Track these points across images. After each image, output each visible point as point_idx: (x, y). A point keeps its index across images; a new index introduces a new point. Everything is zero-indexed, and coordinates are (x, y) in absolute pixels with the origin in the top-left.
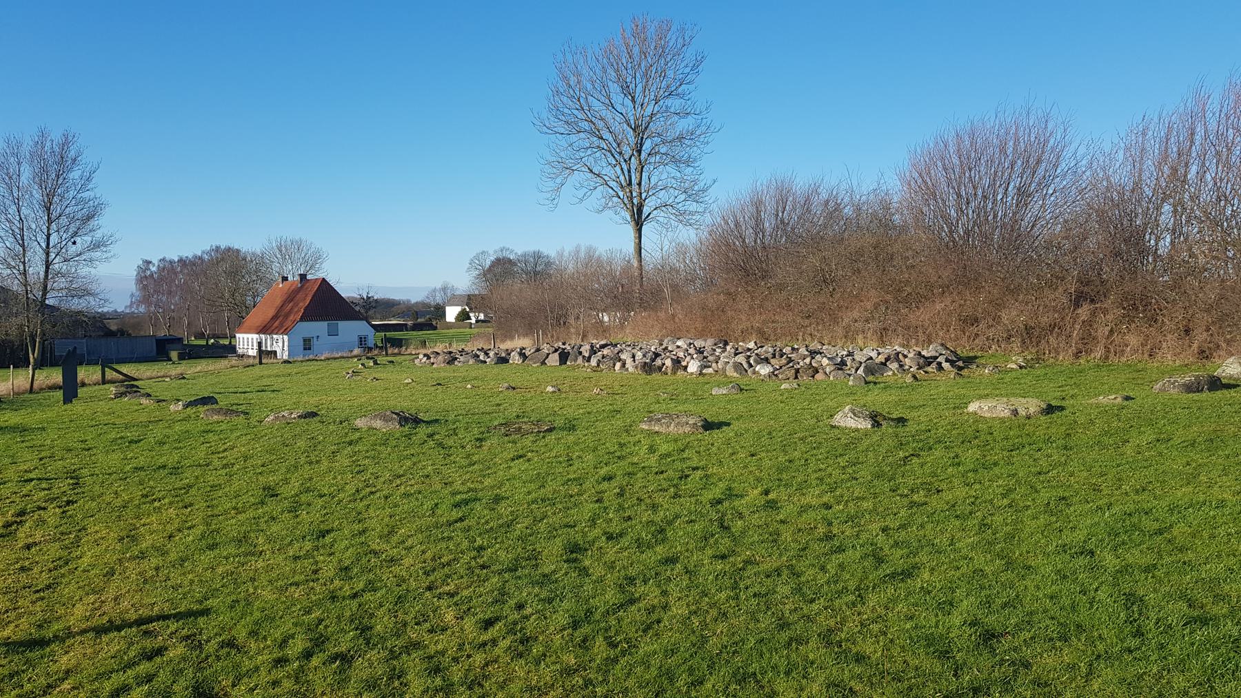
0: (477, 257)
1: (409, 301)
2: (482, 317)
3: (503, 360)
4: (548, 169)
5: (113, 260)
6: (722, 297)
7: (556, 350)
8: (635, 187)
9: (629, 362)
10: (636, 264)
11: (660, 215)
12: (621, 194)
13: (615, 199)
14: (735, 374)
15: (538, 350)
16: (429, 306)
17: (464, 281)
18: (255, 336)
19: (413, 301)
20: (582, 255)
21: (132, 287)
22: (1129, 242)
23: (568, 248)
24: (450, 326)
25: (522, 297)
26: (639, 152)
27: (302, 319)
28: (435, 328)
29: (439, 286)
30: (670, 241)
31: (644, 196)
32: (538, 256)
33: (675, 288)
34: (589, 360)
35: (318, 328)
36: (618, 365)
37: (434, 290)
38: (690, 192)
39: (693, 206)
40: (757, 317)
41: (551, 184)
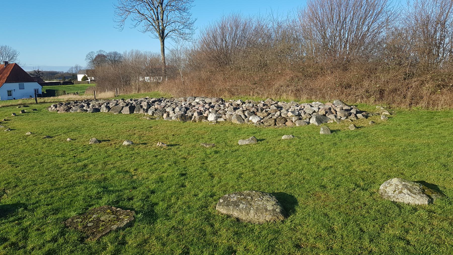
1: (62, 72)
2: (93, 78)
3: (97, 110)
4: (118, 11)
7: (127, 105)
8: (160, 20)
10: (162, 58)
11: (173, 34)
12: (154, 24)
13: (151, 27)
14: (238, 122)
15: (117, 105)
16: (70, 74)
17: (84, 64)
19: (64, 72)
20: (134, 54)
22: (431, 45)
23: (128, 51)
24: (79, 83)
25: (111, 72)
26: (162, 4)
27: (6, 82)
28: (73, 84)
29: (74, 66)
30: (181, 46)
31: (165, 25)
32: (115, 54)
34: (147, 111)
35: (14, 86)
36: (165, 115)
37: (72, 68)
38: (185, 24)
39: (187, 31)
40: (228, 83)
41: (120, 18)
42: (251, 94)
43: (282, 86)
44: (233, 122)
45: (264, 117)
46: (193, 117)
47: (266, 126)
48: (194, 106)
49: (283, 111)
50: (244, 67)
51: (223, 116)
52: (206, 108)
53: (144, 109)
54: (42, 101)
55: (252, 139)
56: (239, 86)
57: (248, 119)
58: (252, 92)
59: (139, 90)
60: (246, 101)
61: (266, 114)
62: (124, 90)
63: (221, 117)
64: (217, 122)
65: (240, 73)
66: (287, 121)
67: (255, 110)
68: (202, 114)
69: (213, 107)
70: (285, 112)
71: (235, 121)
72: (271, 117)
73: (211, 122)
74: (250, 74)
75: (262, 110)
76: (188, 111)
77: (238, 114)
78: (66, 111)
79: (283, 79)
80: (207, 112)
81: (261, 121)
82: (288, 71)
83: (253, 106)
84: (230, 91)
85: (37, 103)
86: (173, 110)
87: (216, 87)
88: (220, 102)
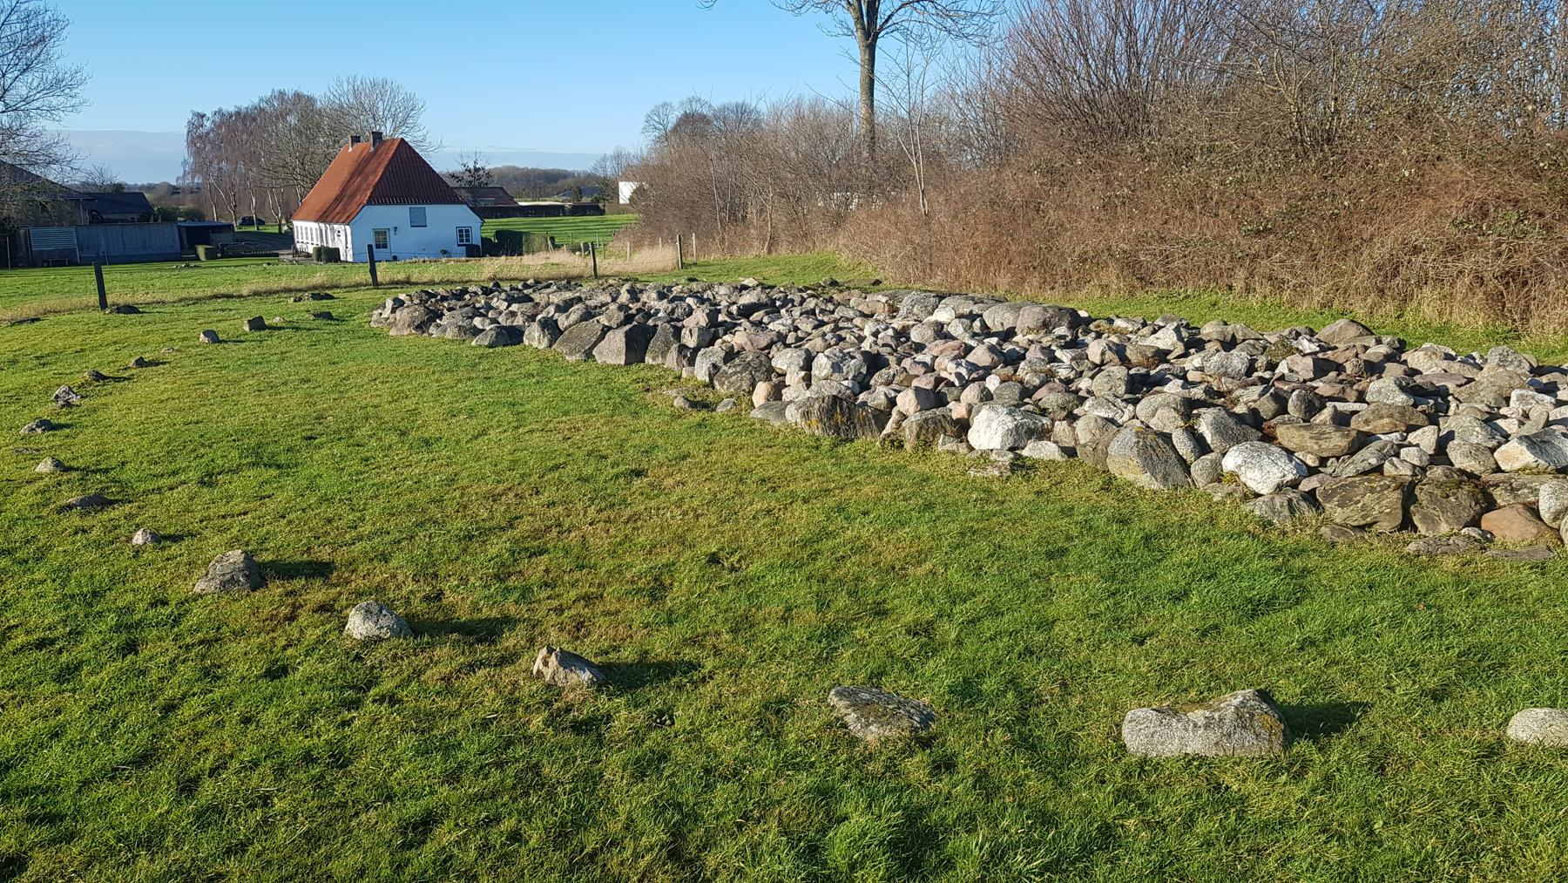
0: (656, 112)
5: (83, 108)
6: (1036, 178)
9: (794, 390)
14: (1145, 480)
17: (637, 142)
18: (315, 225)
21: (182, 152)
24: (622, 210)
27: (371, 201)
28: (602, 212)
29: (610, 152)
32: (742, 111)
33: (933, 158)
35: (395, 215)
36: (762, 390)
37: (604, 159)
40: (1122, 228)
42: (1239, 285)
43: (1416, 250)
44: (1113, 469)
45: (1323, 461)
46: (895, 416)
47: (1343, 528)
48: (920, 348)
49: (1462, 420)
50: (1211, 150)
51: (1061, 427)
52: (973, 367)
53: (683, 348)
54: (401, 276)
55: (1243, 719)
56: (1176, 240)
57: (1217, 465)
58: (1241, 273)
59: (773, 243)
60: (1209, 330)
61: (1337, 441)
62: (722, 241)
63: (1043, 434)
64: (1019, 465)
65: (1188, 177)
66: (1491, 505)
67: (1266, 407)
68: (941, 401)
69: (1014, 359)
70: (1478, 436)
71: (1127, 466)
72: (1378, 469)
73: (985, 456)
74: (1240, 181)
75: (1313, 405)
76: (877, 379)
77: (1154, 423)
78: (418, 327)
79: (1422, 214)
80: (970, 394)
81: (1306, 485)
82: (1455, 167)
83: (1251, 369)
84: (1130, 264)
85: (376, 284)
86: (807, 366)
87: (1063, 243)
88: (1062, 330)
